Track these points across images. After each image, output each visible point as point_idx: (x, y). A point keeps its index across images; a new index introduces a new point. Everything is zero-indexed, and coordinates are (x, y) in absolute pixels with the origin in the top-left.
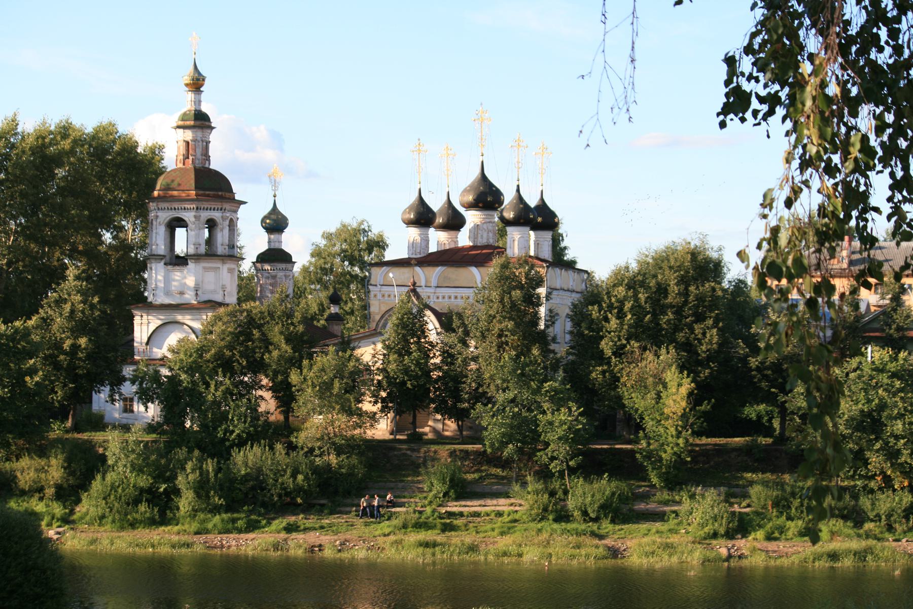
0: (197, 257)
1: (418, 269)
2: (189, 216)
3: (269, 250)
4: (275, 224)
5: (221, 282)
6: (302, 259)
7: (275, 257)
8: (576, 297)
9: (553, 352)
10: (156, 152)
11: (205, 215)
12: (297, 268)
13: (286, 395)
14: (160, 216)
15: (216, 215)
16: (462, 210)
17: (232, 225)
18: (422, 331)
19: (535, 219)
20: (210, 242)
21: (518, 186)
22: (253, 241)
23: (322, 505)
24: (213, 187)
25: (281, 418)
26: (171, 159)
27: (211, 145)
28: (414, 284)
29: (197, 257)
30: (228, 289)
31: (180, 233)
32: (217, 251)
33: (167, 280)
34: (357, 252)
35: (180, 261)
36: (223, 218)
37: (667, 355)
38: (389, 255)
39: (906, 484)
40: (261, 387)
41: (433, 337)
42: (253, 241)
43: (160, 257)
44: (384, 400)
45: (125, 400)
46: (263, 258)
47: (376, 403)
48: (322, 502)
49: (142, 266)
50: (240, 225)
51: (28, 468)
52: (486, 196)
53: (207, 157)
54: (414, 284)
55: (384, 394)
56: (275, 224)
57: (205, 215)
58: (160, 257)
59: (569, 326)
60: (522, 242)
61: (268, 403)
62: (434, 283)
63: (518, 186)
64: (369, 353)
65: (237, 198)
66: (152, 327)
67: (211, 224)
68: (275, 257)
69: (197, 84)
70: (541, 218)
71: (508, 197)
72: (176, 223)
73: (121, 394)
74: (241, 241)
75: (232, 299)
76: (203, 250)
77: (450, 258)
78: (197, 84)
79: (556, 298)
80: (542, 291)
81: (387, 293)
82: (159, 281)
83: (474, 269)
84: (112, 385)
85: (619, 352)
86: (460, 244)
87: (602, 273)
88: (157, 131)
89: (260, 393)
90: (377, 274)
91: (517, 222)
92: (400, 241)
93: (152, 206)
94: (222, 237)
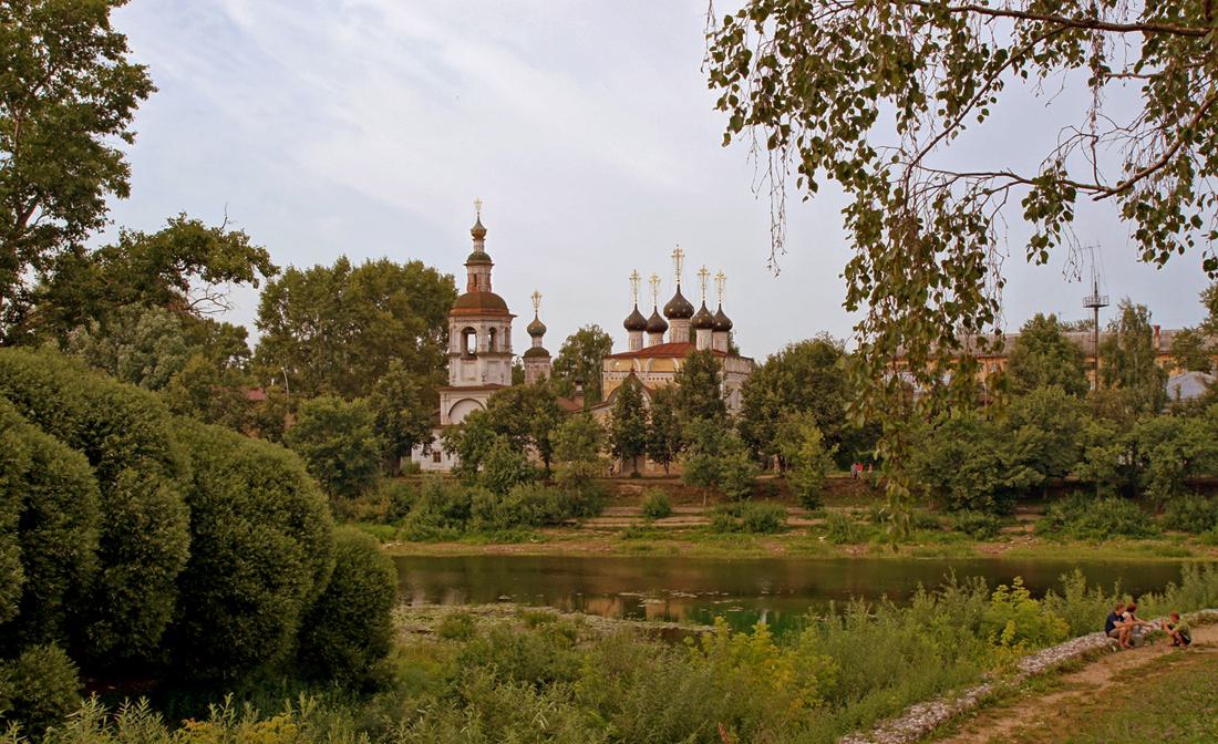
0: (483, 355)
1: (636, 360)
2: (476, 326)
3: (533, 348)
4: (537, 331)
5: (500, 374)
6: (555, 354)
7: (537, 353)
8: (745, 378)
9: (730, 415)
10: (449, 280)
11: (489, 325)
12: (552, 360)
13: (546, 448)
14: (456, 326)
15: (496, 325)
16: (666, 319)
17: (508, 331)
18: (638, 403)
19: (716, 323)
20: (492, 343)
21: (679, 286)
22: (521, 343)
23: (572, 524)
24: (495, 309)
25: (543, 464)
26: (462, 287)
27: (492, 277)
28: (633, 370)
29: (483, 355)
30: (505, 375)
31: (471, 337)
32: (496, 352)
33: (462, 371)
34: (591, 346)
35: (472, 357)
36: (502, 327)
37: (809, 416)
38: (615, 350)
39: (723, 739)
40: (529, 442)
41: (647, 406)
42: (521, 343)
43: (457, 355)
44: (614, 450)
45: (435, 453)
46: (529, 355)
47: (608, 452)
48: (574, 521)
49: (446, 361)
50: (513, 332)
51: (1105, 484)
52: (679, 309)
53: (489, 286)
54: (633, 370)
55: (614, 446)
56: (537, 331)
57: (489, 325)
58: (457, 355)
59: (741, 397)
60: (703, 339)
61: (534, 455)
62: (647, 369)
63: (679, 286)
64: (603, 417)
65: (510, 313)
66: (453, 402)
67: (493, 331)
68: (537, 353)
69: (479, 234)
70: (721, 325)
71: (697, 309)
72: (467, 332)
73: (431, 450)
74: (513, 342)
75: (508, 383)
76: (487, 350)
77: (658, 353)
78: (479, 234)
79: (730, 379)
80: (721, 373)
81: (612, 378)
82: (459, 373)
83: (675, 360)
84: (425, 443)
85: (774, 415)
86: (665, 342)
87: (761, 361)
88: (452, 267)
89: (528, 446)
90: (607, 364)
91: (702, 326)
92: (622, 342)
93: (452, 319)
94: (500, 340)
